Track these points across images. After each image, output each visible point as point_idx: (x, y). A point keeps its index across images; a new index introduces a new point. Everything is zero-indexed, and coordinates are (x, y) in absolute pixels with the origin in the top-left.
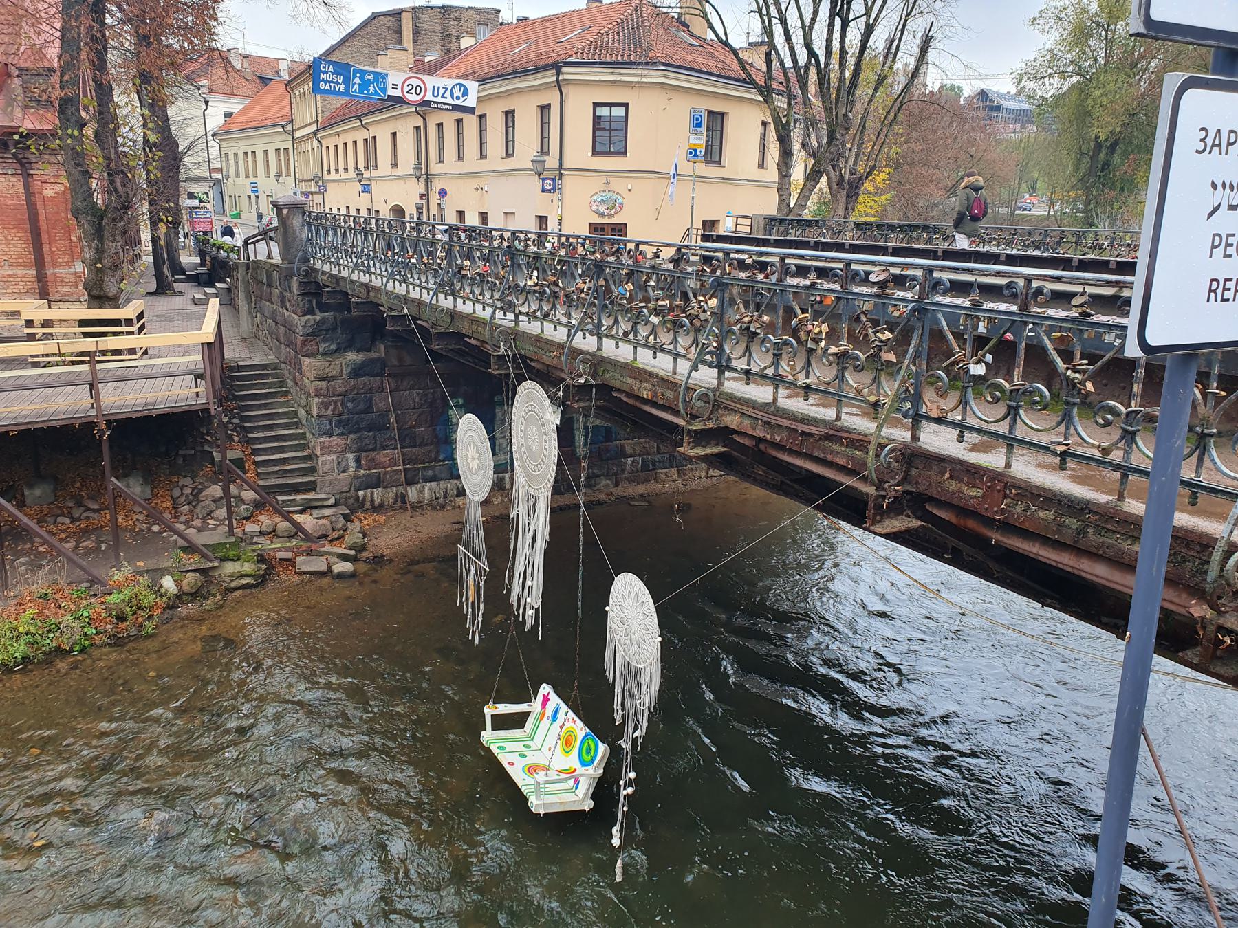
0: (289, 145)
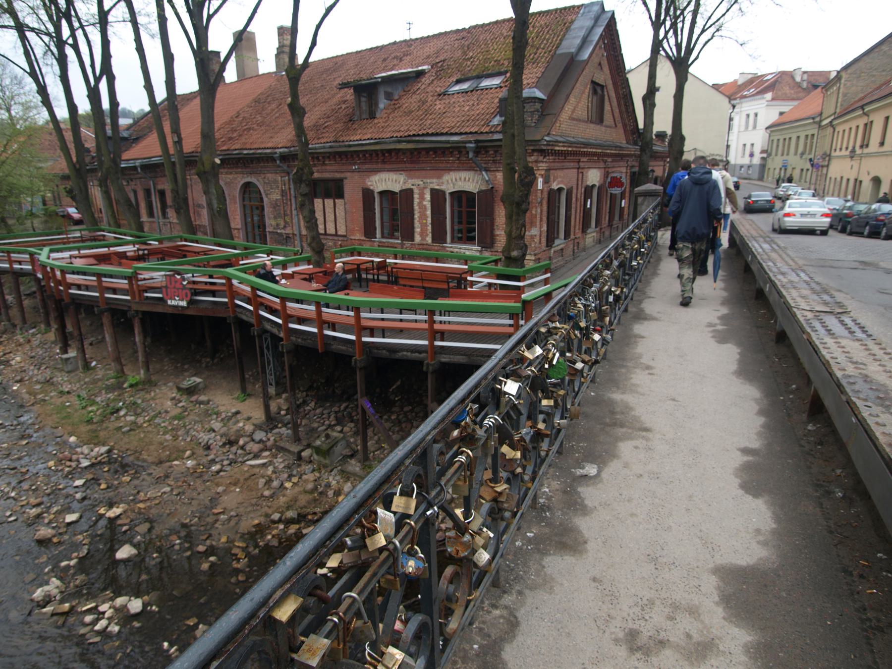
0: (815, 131)
